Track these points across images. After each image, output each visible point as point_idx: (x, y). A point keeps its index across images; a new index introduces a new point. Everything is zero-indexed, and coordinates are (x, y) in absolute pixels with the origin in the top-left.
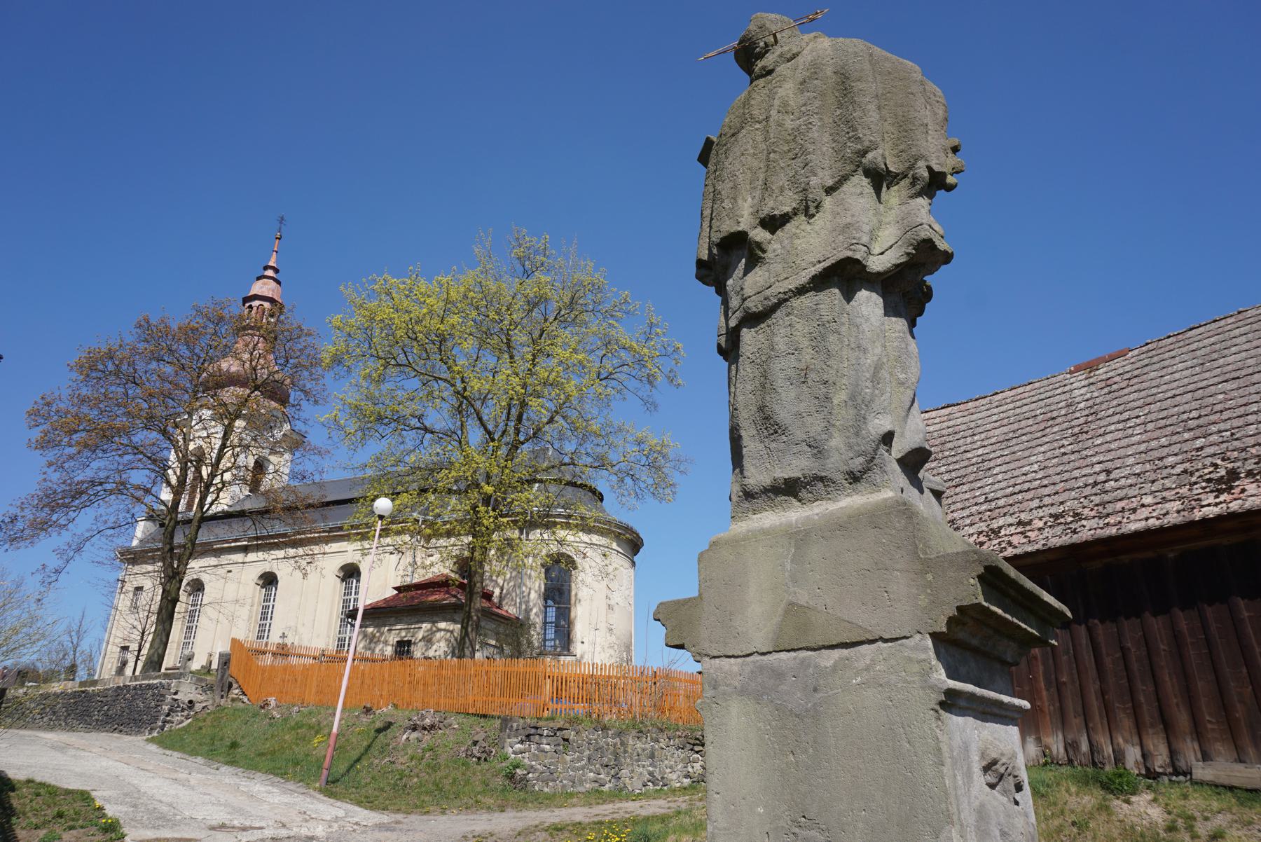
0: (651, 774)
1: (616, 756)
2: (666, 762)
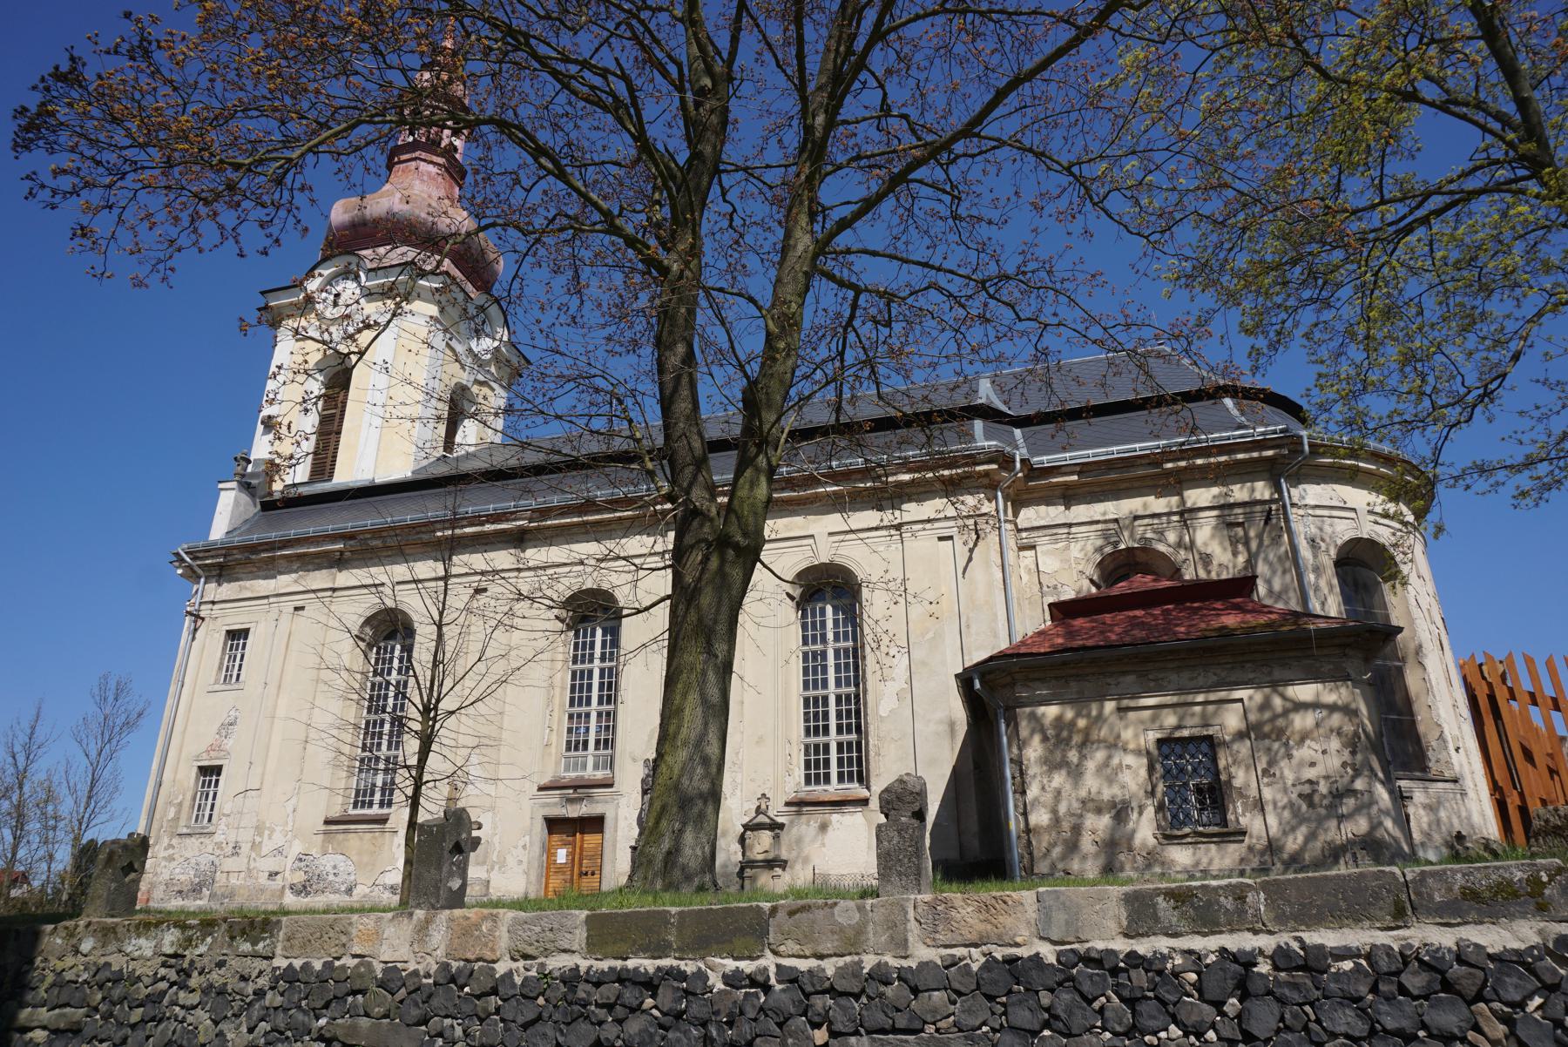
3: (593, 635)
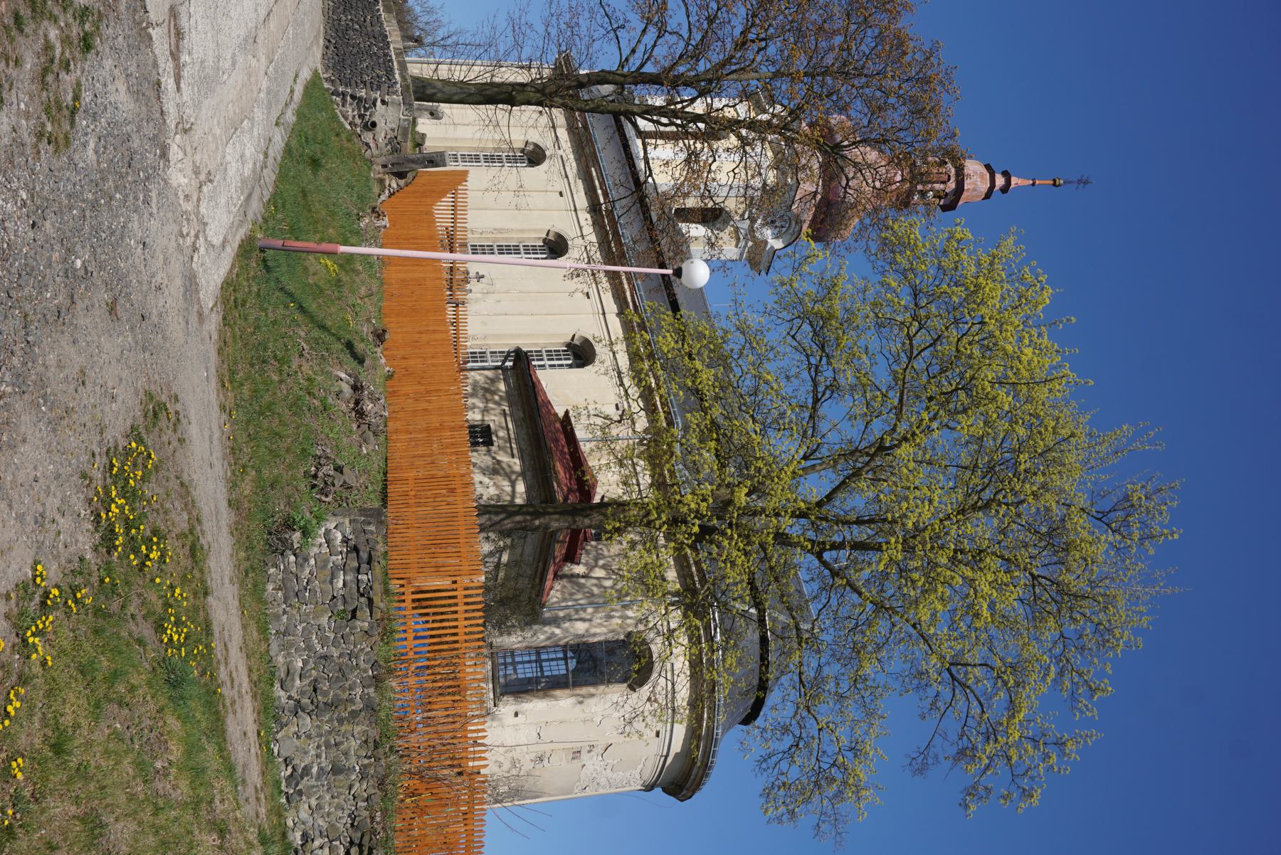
0: (307, 771)
1: (331, 706)
2: (328, 797)
3: (565, 359)
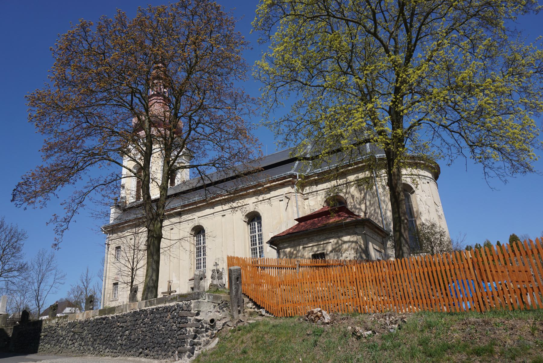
3: (201, 237)
